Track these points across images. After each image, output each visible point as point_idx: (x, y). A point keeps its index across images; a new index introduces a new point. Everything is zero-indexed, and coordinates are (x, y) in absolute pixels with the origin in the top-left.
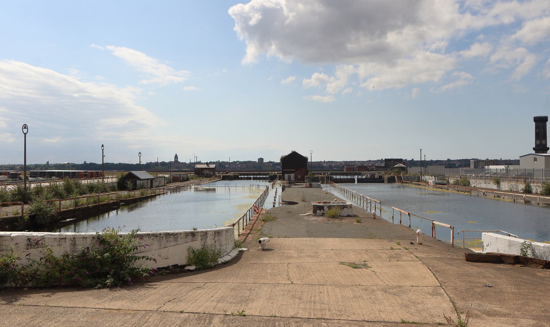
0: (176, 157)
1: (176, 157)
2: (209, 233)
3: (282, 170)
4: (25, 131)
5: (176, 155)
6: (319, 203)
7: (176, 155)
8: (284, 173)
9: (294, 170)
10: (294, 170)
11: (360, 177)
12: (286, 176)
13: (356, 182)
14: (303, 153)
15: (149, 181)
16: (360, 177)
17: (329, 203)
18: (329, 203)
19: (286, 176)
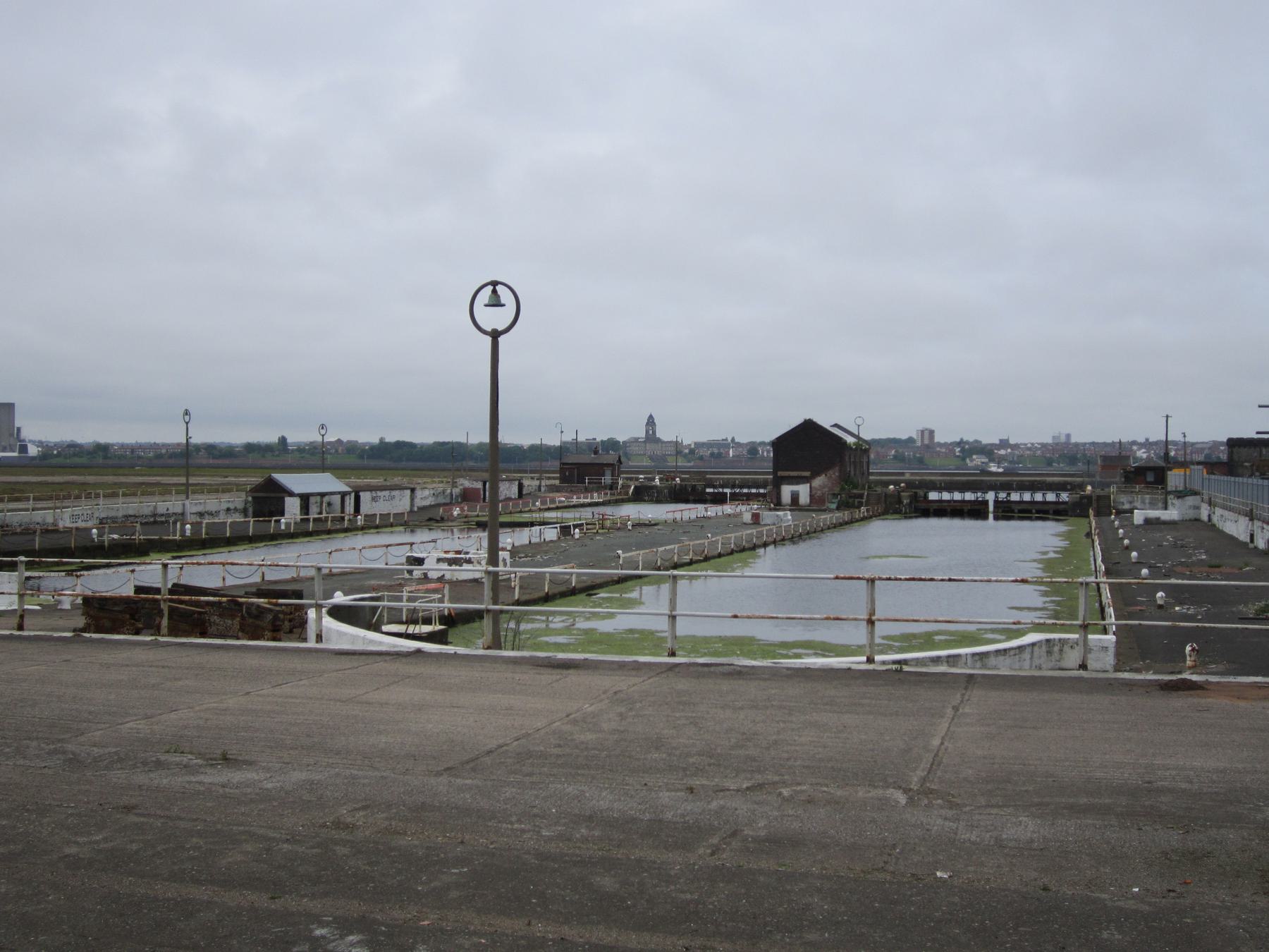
0: (651, 422)
1: (651, 422)
2: (509, 644)
3: (775, 473)
4: (187, 418)
5: (651, 417)
6: (446, 552)
7: (651, 417)
8: (778, 482)
9: (807, 474)
10: (807, 474)
11: (1002, 495)
12: (786, 491)
13: (991, 516)
14: (825, 422)
15: (337, 499)
16: (1002, 495)
17: (467, 553)
18: (467, 553)
19: (786, 491)
